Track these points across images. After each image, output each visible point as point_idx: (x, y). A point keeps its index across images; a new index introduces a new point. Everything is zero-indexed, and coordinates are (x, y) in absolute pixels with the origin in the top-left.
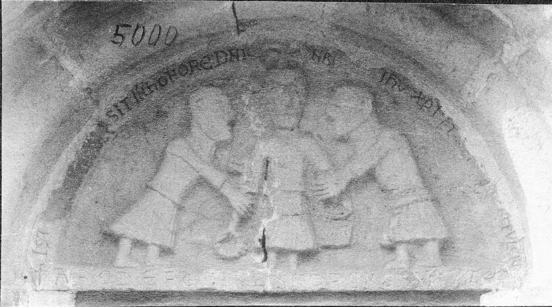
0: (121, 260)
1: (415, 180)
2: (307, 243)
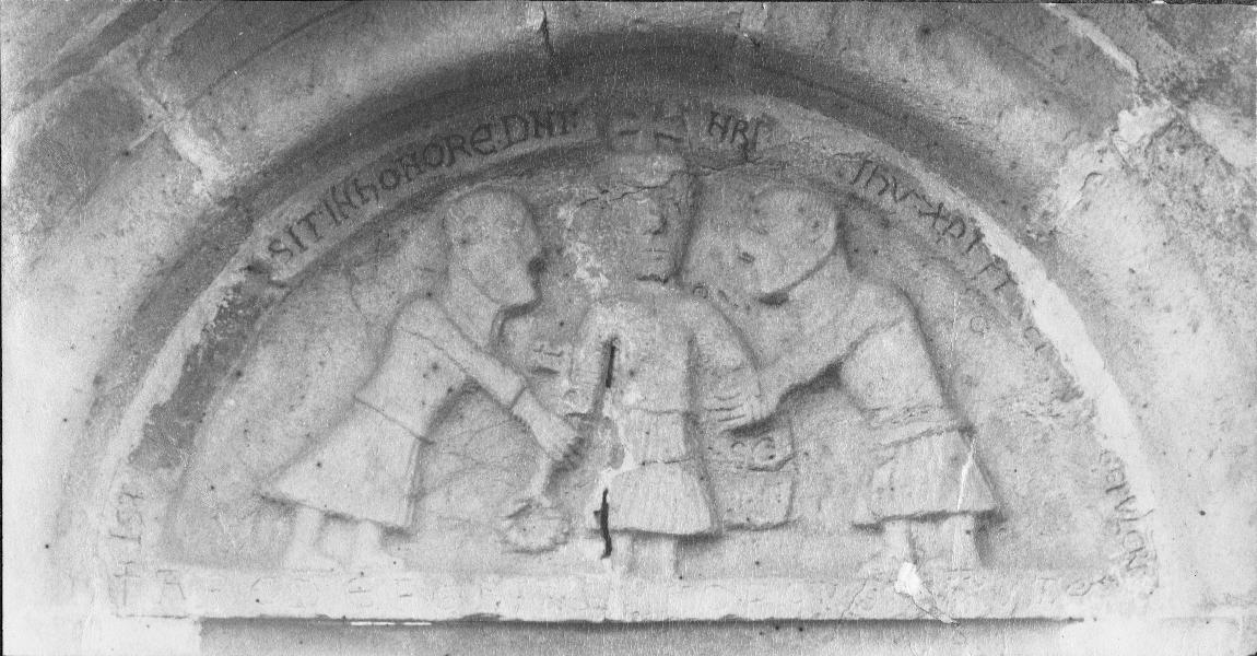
1: (929, 391)
2: (696, 520)
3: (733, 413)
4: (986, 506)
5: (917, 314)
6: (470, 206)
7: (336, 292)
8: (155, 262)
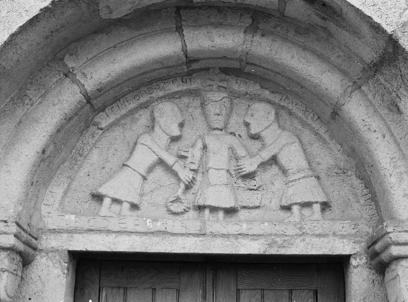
3: (243, 170)
4: (325, 200)
5: (301, 141)
6: (160, 106)
7: (117, 132)
8: (64, 115)
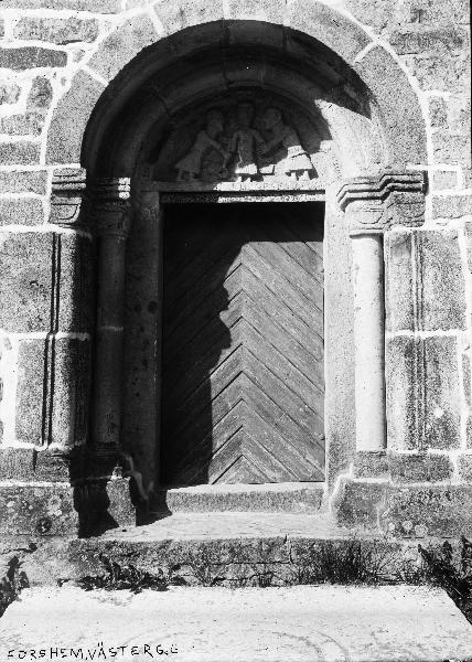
0: (179, 179)
5: (298, 134)
